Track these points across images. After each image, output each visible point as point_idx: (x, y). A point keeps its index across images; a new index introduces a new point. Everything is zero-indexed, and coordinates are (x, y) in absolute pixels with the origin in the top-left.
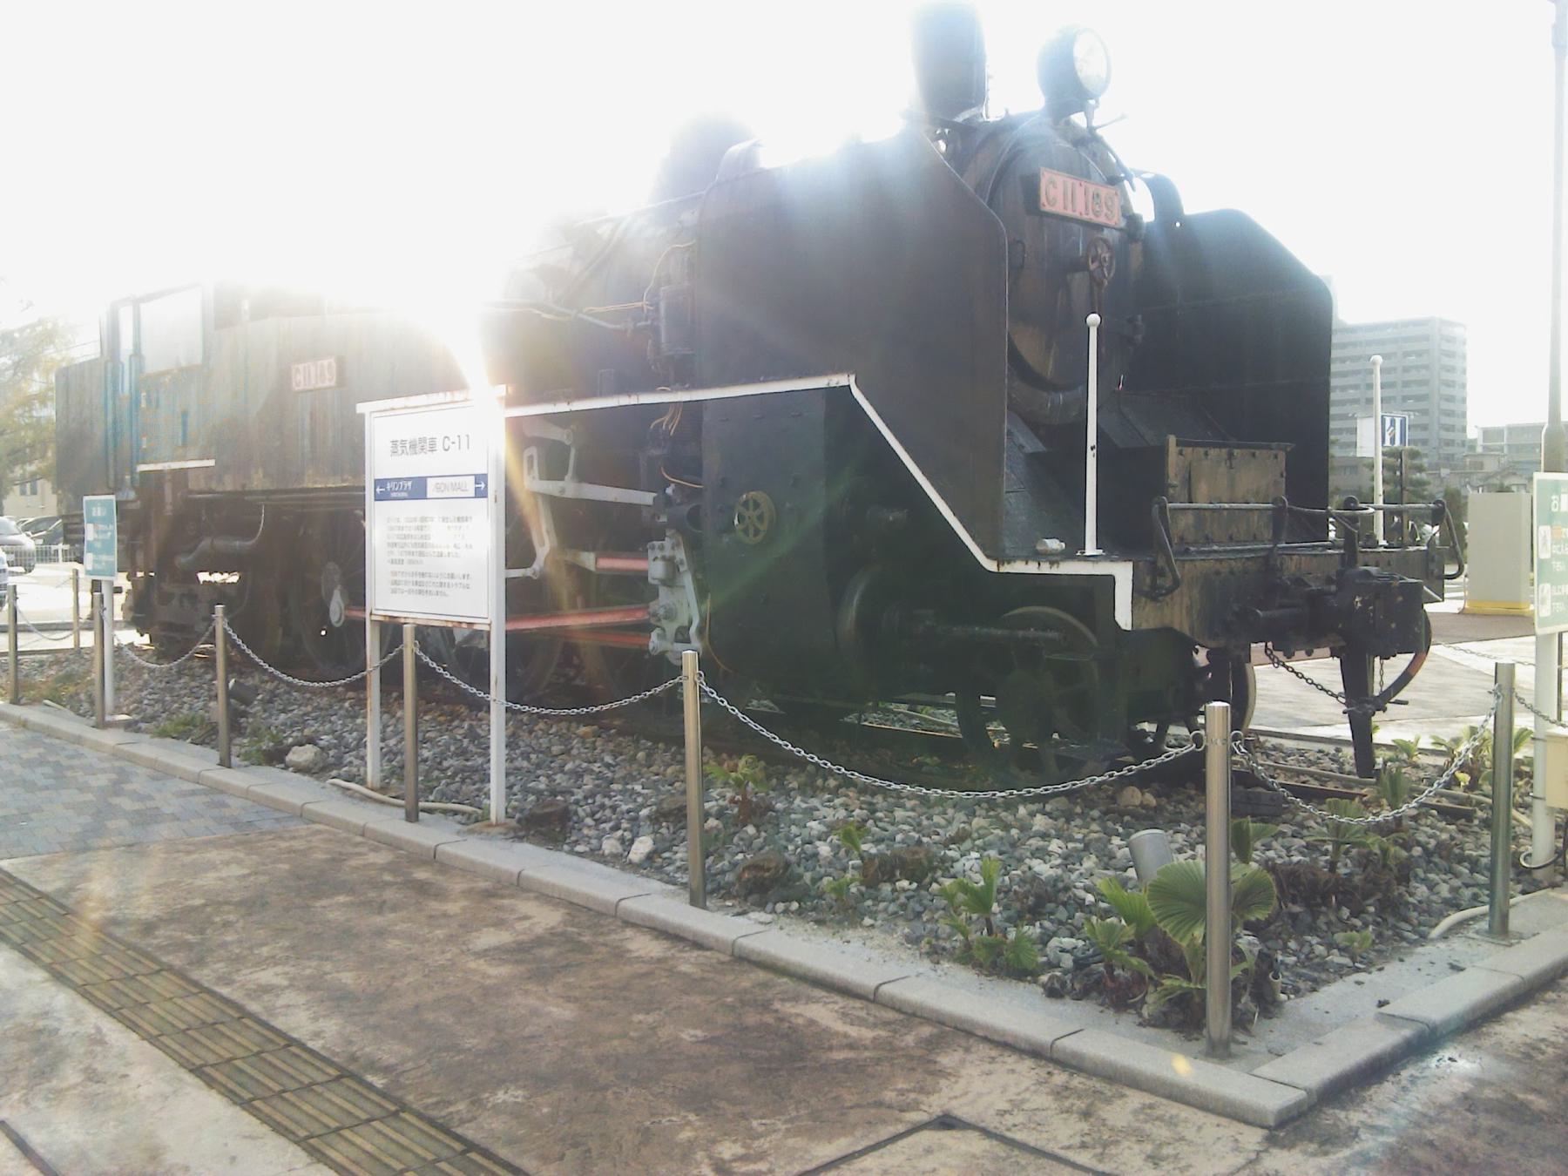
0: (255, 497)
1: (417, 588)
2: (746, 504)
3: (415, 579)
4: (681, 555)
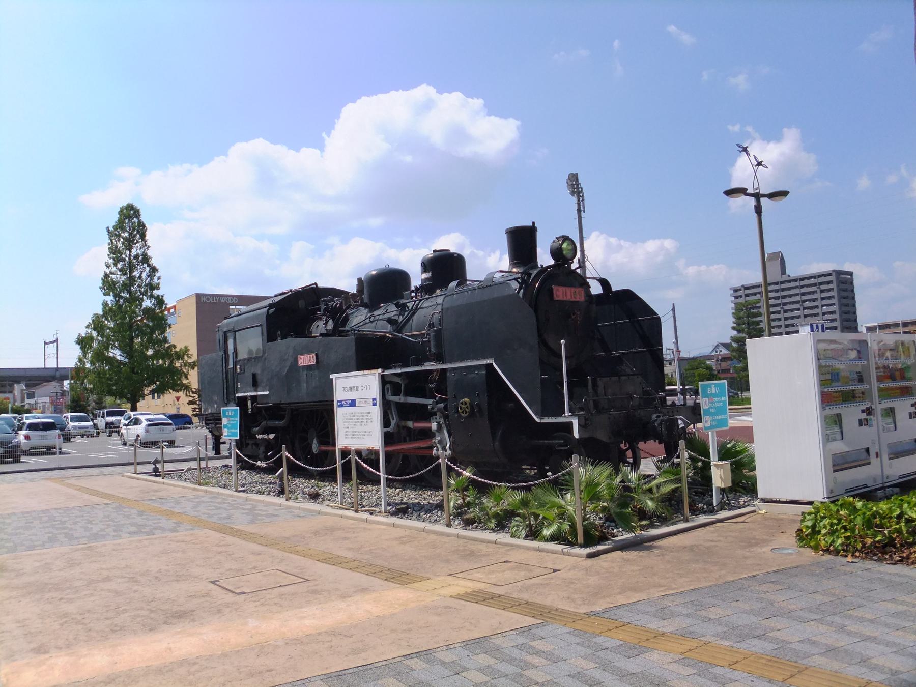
0: (284, 405)
1: (354, 436)
2: (462, 403)
3: (353, 433)
4: (442, 421)
